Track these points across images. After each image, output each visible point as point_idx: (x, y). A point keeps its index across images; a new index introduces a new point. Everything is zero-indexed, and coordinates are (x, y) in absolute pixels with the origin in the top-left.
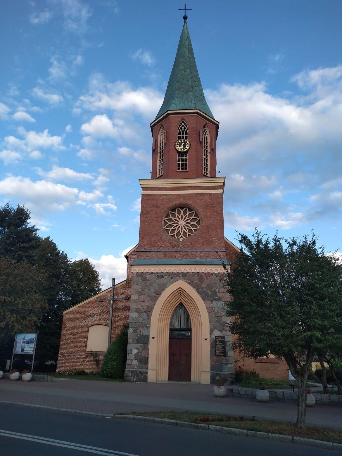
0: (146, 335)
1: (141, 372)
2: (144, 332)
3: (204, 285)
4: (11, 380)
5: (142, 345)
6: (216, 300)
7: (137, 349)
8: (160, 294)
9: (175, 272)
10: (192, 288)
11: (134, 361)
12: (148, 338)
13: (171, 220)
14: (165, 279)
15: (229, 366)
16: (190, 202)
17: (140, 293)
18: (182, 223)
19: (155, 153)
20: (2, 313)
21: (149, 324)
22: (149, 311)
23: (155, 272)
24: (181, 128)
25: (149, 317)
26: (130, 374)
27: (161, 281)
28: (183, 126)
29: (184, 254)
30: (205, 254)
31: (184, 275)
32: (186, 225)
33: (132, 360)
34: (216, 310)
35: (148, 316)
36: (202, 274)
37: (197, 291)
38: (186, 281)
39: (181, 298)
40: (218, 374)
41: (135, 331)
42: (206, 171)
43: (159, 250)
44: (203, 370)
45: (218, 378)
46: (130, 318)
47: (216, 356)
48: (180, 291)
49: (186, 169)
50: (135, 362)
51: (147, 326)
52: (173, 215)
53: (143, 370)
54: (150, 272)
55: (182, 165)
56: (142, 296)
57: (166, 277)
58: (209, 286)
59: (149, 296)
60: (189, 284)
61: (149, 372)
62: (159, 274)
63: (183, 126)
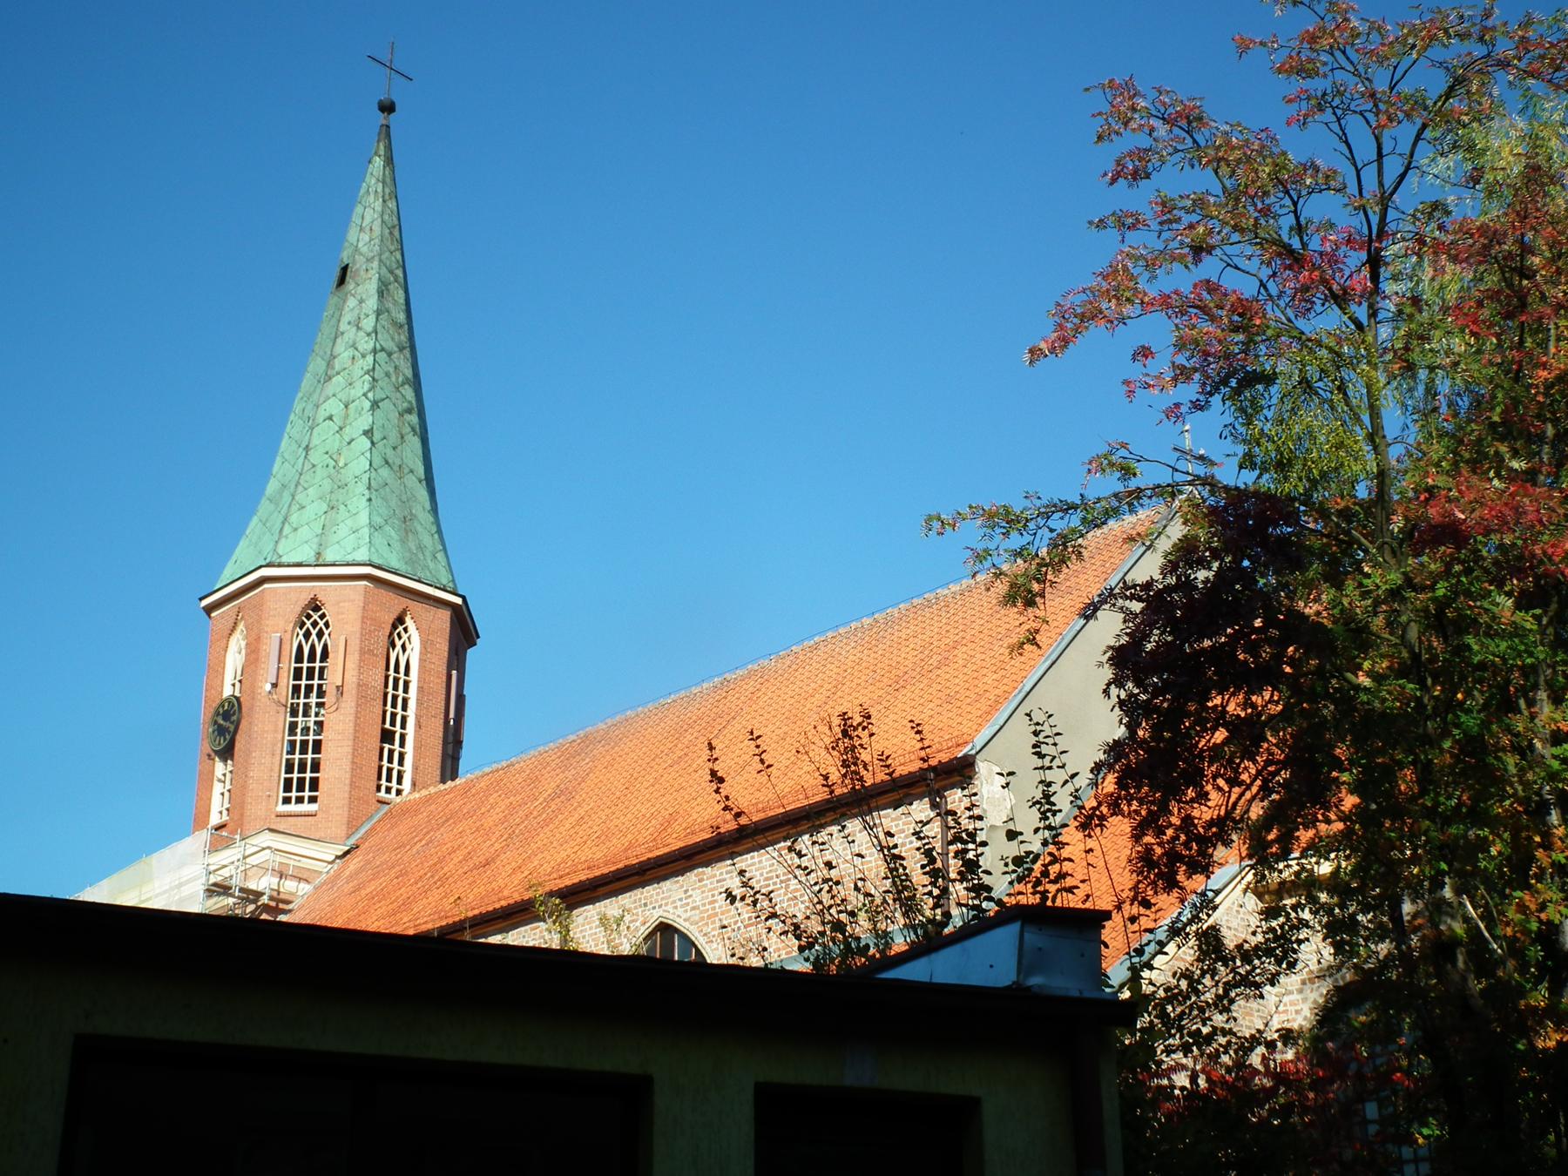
24: (307, 635)
28: (315, 624)
55: (301, 788)
63: (315, 624)
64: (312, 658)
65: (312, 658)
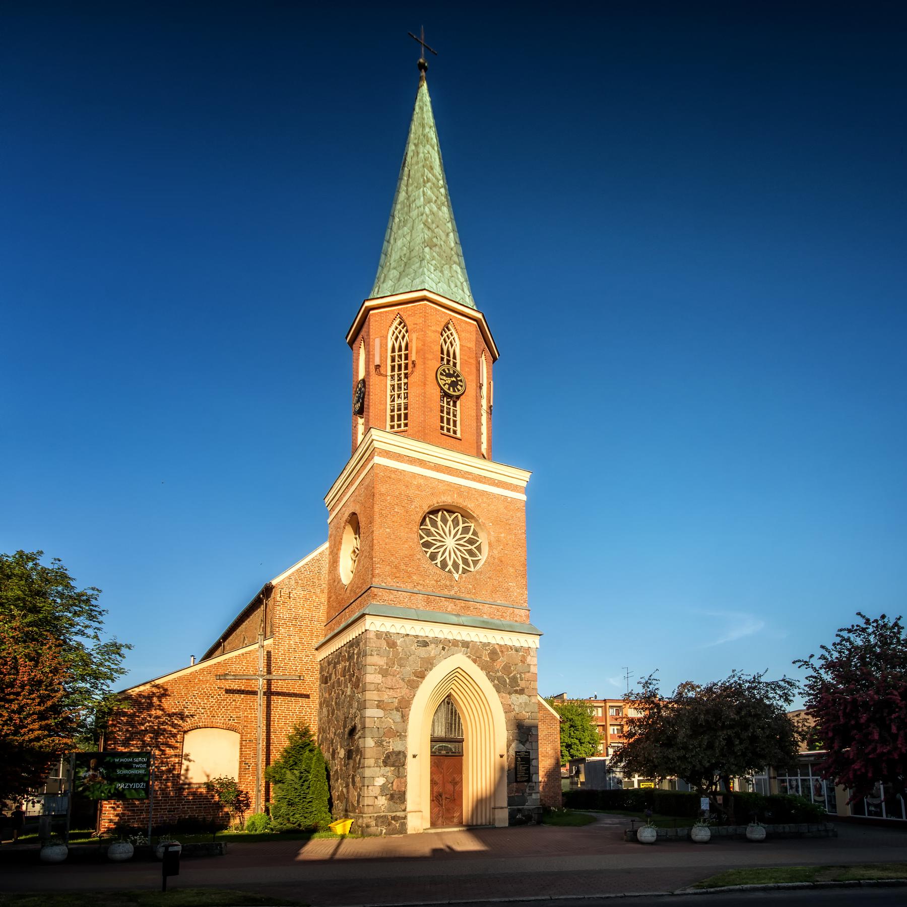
0: (399, 752)
1: (394, 818)
2: (394, 745)
3: (499, 664)
4: (642, 843)
5: (392, 768)
6: (516, 692)
7: (383, 776)
8: (423, 677)
9: (450, 637)
10: (479, 669)
11: (379, 798)
12: (405, 757)
13: (429, 533)
14: (432, 650)
15: (534, 796)
16: (470, 505)
17: (384, 673)
18: (450, 543)
19: (381, 375)
20: (629, 775)
21: (405, 731)
22: (403, 707)
23: (412, 633)
25: (404, 718)
26: (373, 823)
27: (422, 652)
29: (463, 605)
30: (498, 610)
31: (466, 644)
32: (454, 537)
33: (376, 797)
34: (517, 709)
35: (403, 716)
36: (496, 647)
37: (488, 675)
38: (469, 657)
39: (453, 686)
40: (519, 811)
41: (379, 744)
42: (451, 427)
43: (415, 590)
44: (497, 806)
45: (519, 816)
46: (367, 720)
47: (516, 781)
48: (457, 674)
49: (406, 425)
50: (382, 801)
51: (401, 735)
52: (434, 524)
53: (398, 814)
54: (403, 632)
56: (389, 678)
57: (433, 646)
58: (507, 668)
59: (403, 680)
60: (475, 661)
61: (409, 816)
62: (420, 639)
64: (400, 350)
65: (400, 350)
